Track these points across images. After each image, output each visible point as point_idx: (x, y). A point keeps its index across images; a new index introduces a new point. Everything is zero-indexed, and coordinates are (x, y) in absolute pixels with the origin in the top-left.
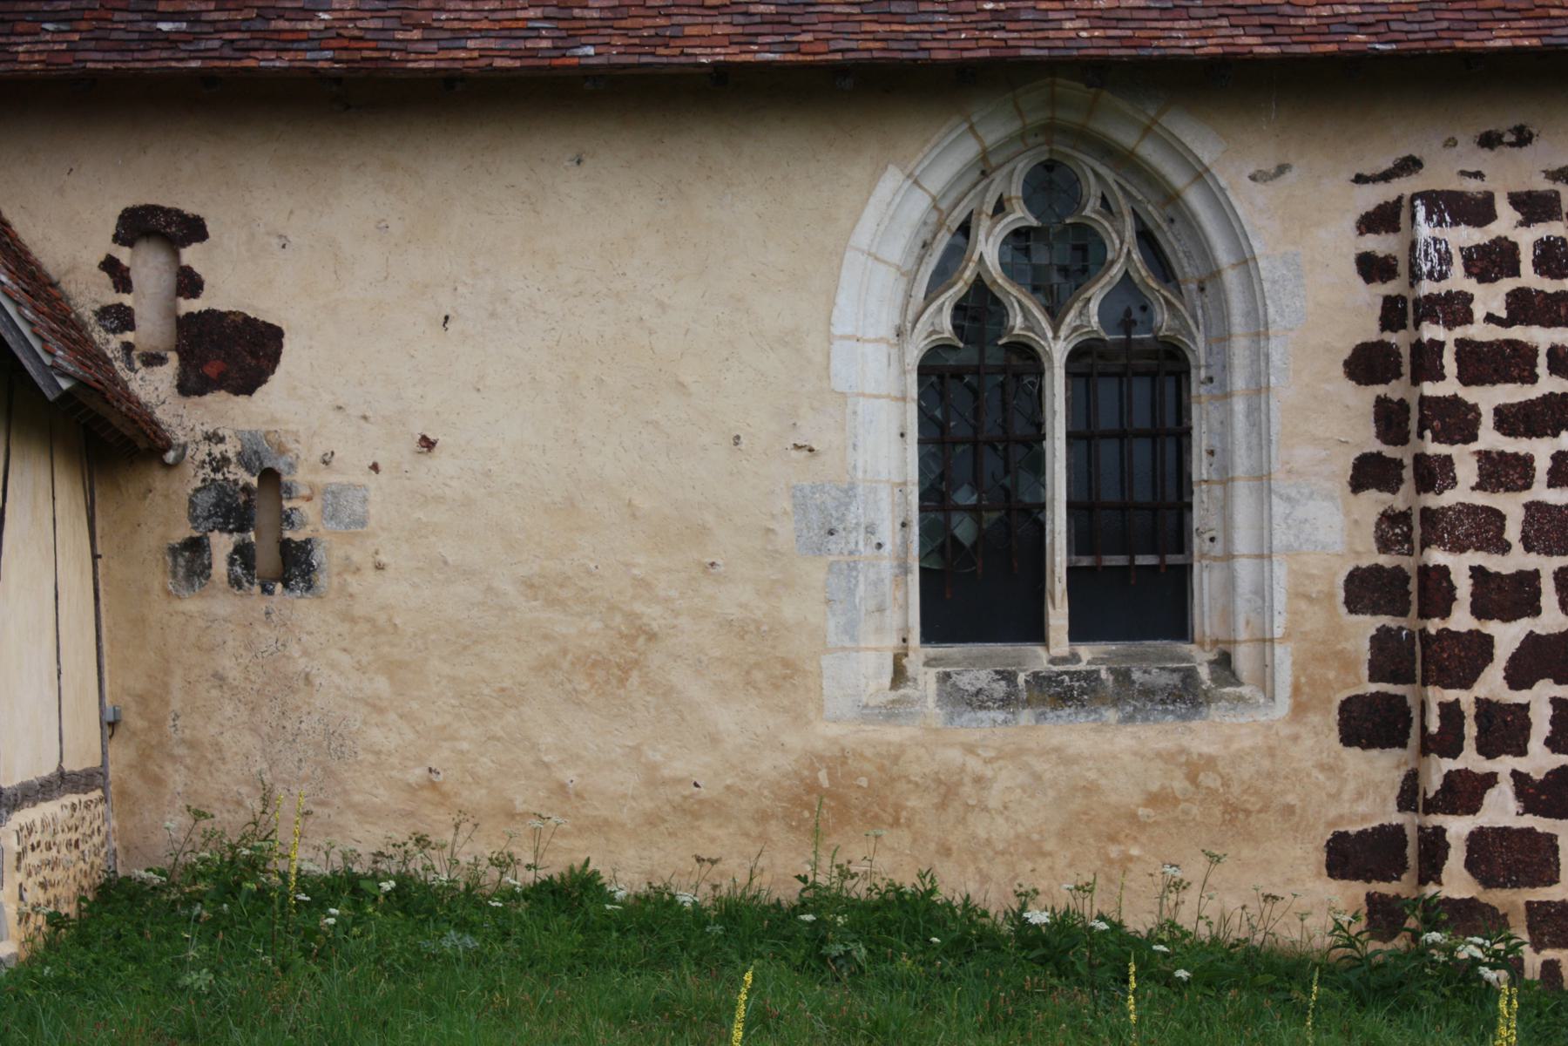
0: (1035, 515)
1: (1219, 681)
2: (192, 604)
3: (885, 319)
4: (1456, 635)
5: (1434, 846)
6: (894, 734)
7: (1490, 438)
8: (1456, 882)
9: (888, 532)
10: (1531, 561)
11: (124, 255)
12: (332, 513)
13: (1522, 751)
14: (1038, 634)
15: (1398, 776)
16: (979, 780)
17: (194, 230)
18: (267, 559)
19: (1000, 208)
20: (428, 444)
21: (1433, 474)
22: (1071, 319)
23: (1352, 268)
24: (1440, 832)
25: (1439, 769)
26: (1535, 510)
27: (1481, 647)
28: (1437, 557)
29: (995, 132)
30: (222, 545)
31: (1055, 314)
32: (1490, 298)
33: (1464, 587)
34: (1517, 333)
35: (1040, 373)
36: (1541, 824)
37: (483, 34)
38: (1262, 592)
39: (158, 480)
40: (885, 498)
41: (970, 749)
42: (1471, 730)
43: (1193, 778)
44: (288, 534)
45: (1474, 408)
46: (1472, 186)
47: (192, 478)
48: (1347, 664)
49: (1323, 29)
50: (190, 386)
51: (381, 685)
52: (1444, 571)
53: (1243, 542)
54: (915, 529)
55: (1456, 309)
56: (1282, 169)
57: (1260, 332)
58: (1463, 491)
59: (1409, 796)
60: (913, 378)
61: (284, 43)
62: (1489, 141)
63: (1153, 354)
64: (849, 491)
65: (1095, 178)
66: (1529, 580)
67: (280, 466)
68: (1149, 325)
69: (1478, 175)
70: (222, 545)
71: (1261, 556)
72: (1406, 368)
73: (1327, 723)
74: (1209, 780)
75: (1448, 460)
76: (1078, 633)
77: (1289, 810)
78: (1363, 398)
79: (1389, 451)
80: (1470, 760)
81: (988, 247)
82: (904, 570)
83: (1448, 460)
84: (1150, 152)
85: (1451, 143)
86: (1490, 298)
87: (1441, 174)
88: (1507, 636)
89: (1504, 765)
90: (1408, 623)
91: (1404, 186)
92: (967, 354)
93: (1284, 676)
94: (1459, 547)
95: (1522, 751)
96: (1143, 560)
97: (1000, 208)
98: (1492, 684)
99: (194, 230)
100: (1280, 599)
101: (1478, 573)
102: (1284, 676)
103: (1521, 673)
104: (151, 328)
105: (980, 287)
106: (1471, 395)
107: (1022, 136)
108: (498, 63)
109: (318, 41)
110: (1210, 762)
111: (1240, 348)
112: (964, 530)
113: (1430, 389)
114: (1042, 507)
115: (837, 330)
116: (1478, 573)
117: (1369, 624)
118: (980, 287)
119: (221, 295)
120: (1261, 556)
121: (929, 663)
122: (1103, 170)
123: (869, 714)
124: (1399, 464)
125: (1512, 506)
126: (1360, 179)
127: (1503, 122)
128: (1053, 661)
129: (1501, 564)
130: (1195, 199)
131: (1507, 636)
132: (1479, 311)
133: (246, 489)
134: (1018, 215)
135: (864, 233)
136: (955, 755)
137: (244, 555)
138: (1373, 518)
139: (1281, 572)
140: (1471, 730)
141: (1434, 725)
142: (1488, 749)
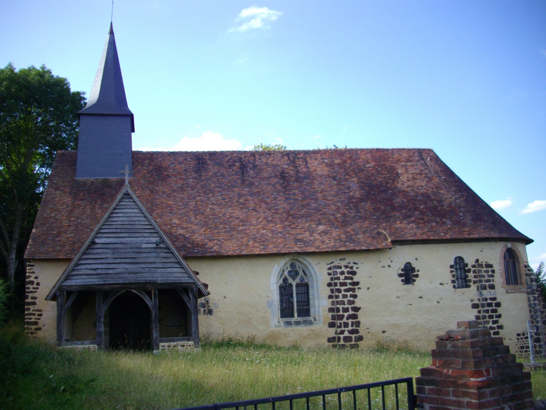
0: (292, 303)
1: (314, 321)
3: (275, 282)
4: (340, 315)
5: (339, 339)
6: (279, 329)
7: (343, 293)
8: (342, 342)
9: (277, 306)
10: (488, 308)
13: (348, 327)
14: (293, 316)
15: (335, 331)
16: (289, 333)
18: (207, 311)
19: (287, 268)
20: (225, 297)
21: (337, 297)
22: (296, 281)
23: (327, 274)
24: (340, 337)
26: (348, 301)
27: (343, 316)
28: (338, 306)
32: (342, 277)
33: (341, 309)
34: (345, 281)
35: (292, 287)
37: (232, 251)
38: (319, 311)
40: (277, 302)
41: (288, 330)
42: (343, 325)
43: (312, 332)
44: (209, 308)
45: (341, 289)
46: (339, 265)
52: (339, 308)
53: (316, 305)
54: (279, 305)
55: (338, 278)
56: (319, 263)
57: (317, 281)
58: (341, 299)
59: (336, 333)
60: (278, 288)
62: (341, 260)
63: (304, 284)
65: (298, 264)
66: (348, 308)
67: (208, 300)
68: (304, 281)
69: (340, 263)
71: (318, 307)
72: (333, 285)
73: (327, 325)
74: (314, 332)
75: (339, 295)
76: (299, 316)
77: (323, 335)
78: (329, 289)
79: (332, 294)
80: (343, 328)
81: (286, 273)
82: (278, 310)
83: (339, 295)
84: (304, 262)
85: (337, 260)
86: (342, 277)
87: (336, 264)
88: (346, 314)
89: (346, 329)
90: (335, 314)
91: (332, 265)
92: (284, 285)
93: (322, 320)
94: (340, 305)
95: (348, 327)
96: (305, 308)
97: (287, 268)
98: (345, 320)
100: (321, 312)
101: (343, 308)
102: (322, 320)
103: (348, 318)
107: (290, 260)
108: (234, 254)
110: (314, 330)
111: (315, 284)
113: (336, 287)
114: (293, 302)
115: (271, 283)
116: (343, 308)
117: (331, 314)
120: (318, 307)
121: (282, 320)
122: (299, 264)
123: (276, 326)
124: (333, 296)
125: (346, 300)
126: (327, 264)
128: (296, 319)
129: (491, 308)
130: (309, 267)
131: (346, 314)
132: (341, 278)
133: (205, 303)
134: (290, 269)
136: (286, 331)
137: (204, 311)
138: (331, 302)
139: (321, 308)
140: (343, 325)
141: (339, 325)
142: (345, 327)
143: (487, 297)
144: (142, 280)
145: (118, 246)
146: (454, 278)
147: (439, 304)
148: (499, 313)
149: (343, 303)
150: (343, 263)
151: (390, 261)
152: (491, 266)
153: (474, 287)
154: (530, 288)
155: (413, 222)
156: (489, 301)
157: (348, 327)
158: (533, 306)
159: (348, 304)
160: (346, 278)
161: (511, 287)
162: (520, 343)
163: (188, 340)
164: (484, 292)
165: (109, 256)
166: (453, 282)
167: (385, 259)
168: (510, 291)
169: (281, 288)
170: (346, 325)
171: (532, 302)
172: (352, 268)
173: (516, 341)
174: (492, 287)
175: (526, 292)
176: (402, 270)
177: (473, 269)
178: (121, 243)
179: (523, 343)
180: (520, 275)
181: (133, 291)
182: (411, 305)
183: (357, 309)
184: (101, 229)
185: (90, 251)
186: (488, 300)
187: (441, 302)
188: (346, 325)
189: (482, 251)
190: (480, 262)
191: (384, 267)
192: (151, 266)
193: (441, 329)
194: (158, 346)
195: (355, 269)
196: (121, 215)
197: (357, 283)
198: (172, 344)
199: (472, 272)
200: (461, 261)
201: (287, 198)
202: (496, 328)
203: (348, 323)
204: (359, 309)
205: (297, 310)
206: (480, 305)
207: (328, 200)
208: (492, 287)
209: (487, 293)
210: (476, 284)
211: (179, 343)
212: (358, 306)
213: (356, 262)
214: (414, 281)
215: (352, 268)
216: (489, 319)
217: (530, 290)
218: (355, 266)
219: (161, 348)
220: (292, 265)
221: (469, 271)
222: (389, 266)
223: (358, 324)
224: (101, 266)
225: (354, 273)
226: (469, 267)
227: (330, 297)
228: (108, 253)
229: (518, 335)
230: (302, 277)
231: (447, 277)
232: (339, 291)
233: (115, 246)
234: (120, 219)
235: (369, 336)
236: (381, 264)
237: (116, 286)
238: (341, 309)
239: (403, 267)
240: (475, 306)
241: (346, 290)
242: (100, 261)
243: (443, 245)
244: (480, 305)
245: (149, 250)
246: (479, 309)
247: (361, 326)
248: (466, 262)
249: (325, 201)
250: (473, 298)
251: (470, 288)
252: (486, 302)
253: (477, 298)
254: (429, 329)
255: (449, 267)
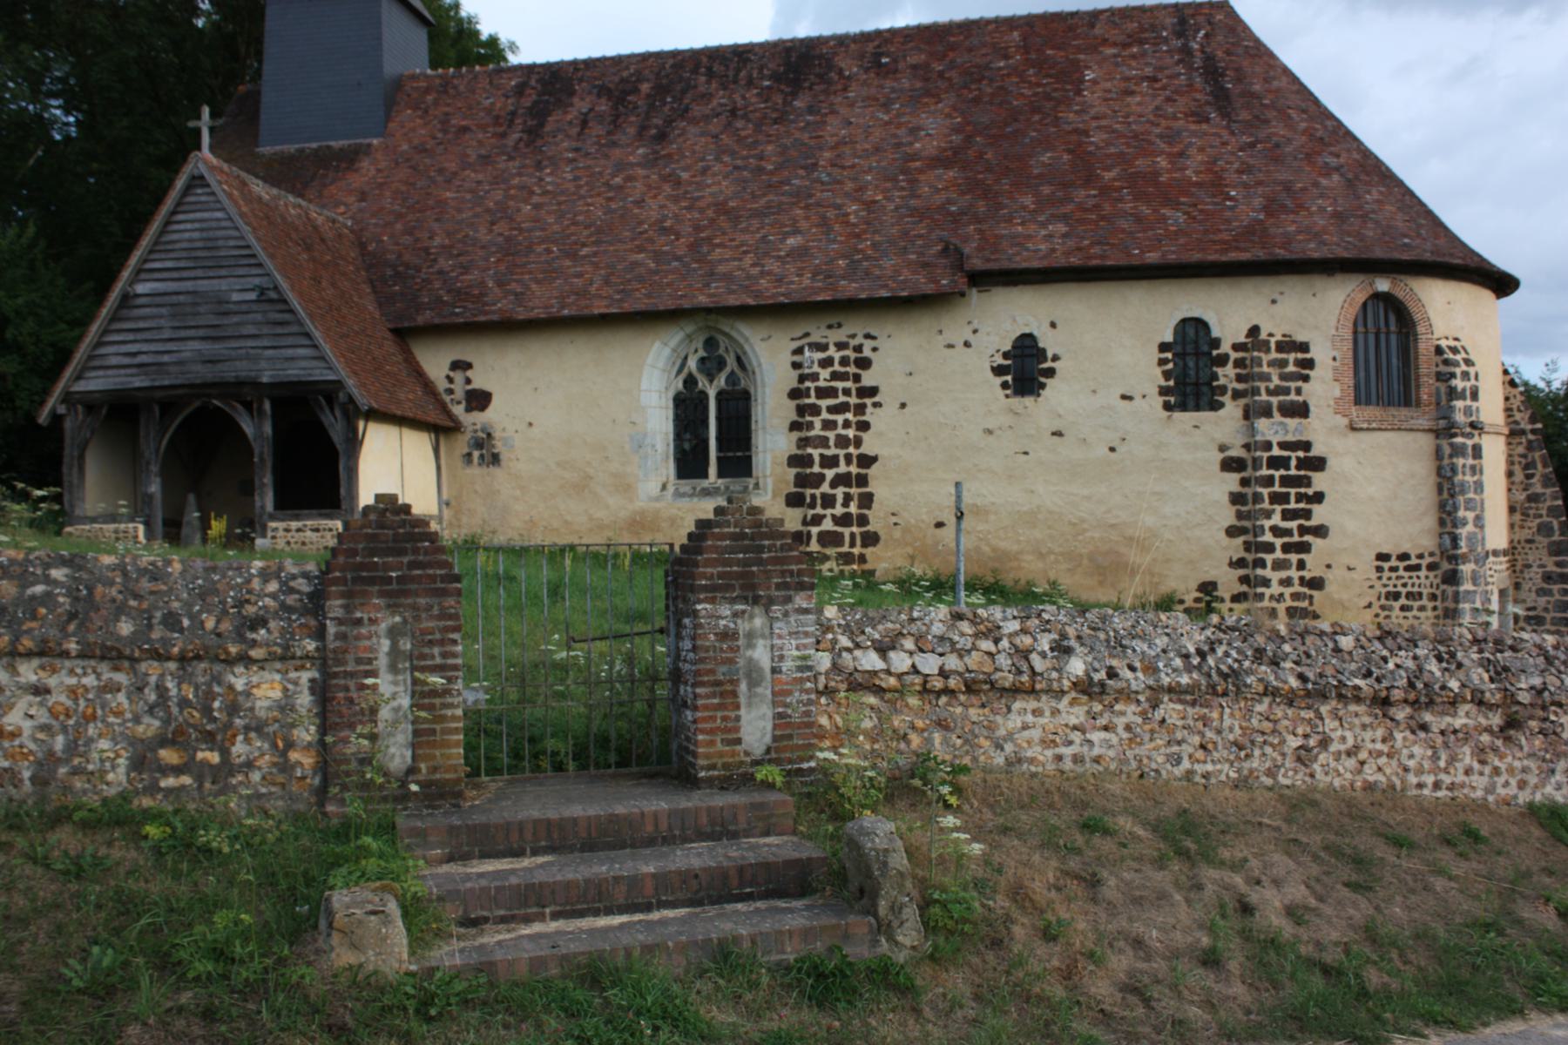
2: (469, 471)
6: (658, 505)
7: (825, 415)
8: (814, 547)
10: (1271, 472)
11: (452, 374)
12: (505, 445)
14: (706, 476)
17: (469, 366)
18: (488, 458)
20: (531, 424)
21: (810, 426)
25: (811, 512)
26: (838, 436)
27: (822, 477)
28: (810, 450)
29: (690, 328)
30: (476, 454)
31: (711, 381)
32: (825, 374)
33: (817, 459)
34: (833, 384)
36: (839, 529)
39: (460, 437)
42: (819, 501)
46: (824, 341)
47: (468, 436)
48: (787, 483)
49: (774, 296)
50: (469, 409)
51: (518, 492)
57: (764, 386)
58: (817, 431)
59: (805, 523)
61: (486, 313)
62: (830, 327)
64: (645, 435)
65: (722, 340)
66: (836, 457)
70: (476, 454)
73: (782, 500)
76: (721, 475)
78: (793, 404)
80: (819, 510)
81: (692, 364)
84: (734, 334)
86: (825, 374)
87: (815, 338)
88: (830, 474)
89: (829, 512)
94: (815, 447)
98: (825, 488)
99: (469, 366)
101: (822, 456)
103: (834, 485)
104: (459, 393)
105: (690, 375)
106: (819, 402)
109: (494, 312)
112: (687, 446)
116: (822, 456)
117: (794, 471)
118: (690, 375)
119: (476, 385)
123: (651, 499)
125: (831, 435)
127: (834, 321)
129: (1282, 472)
131: (830, 474)
134: (702, 353)
135: (649, 361)
136: (674, 511)
137: (482, 456)
140: (819, 501)
142: (824, 506)
143: (1268, 438)
144: (230, 376)
145: (182, 298)
146: (1167, 379)
147: (1112, 455)
148: (1318, 489)
149: (824, 442)
150: (839, 335)
151: (969, 330)
152: (1304, 347)
153: (1232, 409)
154: (1444, 418)
155: (1065, 218)
156: (1276, 452)
157: (833, 507)
158: (1449, 474)
159: (836, 446)
160: (835, 376)
161: (1372, 412)
162: (1384, 581)
163: (330, 517)
164: (1262, 424)
165: (162, 322)
166: (1163, 391)
167: (954, 326)
168: (1365, 426)
169: (679, 401)
170: (829, 501)
171: (1446, 462)
172: (858, 349)
173: (1374, 575)
174: (1301, 410)
175: (1430, 430)
176: (1006, 355)
177: (1234, 355)
178: (188, 293)
179: (1399, 582)
180: (1418, 377)
181: (215, 402)
182: (1026, 453)
183: (867, 461)
184: (146, 261)
185: (124, 312)
186: (1275, 447)
187: (1121, 449)
188: (829, 501)
189: (1274, 302)
190: (1263, 336)
191: (950, 346)
192: (250, 343)
193: (1112, 526)
194: (264, 528)
195: (867, 352)
196: (189, 226)
197: (873, 391)
198: (294, 525)
199: (1230, 364)
200: (1202, 334)
201: (736, 168)
202: (1295, 532)
203: (834, 496)
204: (874, 459)
205: (719, 459)
206: (1249, 463)
207: (843, 168)
208: (1301, 410)
209: (1272, 429)
210: (1243, 401)
211: (309, 523)
212: (871, 453)
213: (873, 333)
214: (1043, 386)
215: (858, 349)
216: (1271, 503)
217: (1442, 423)
218: (868, 344)
219: (270, 534)
220: (710, 344)
221: (1222, 360)
222: (967, 344)
223: (867, 500)
224: (145, 347)
225: (864, 363)
226: (1225, 348)
227: (795, 426)
228: (161, 317)
229: (1383, 557)
230: (732, 373)
231: (1149, 375)
232: (815, 410)
233: (174, 299)
234: (187, 235)
235: (897, 534)
236: (941, 340)
237: (180, 392)
238: (817, 459)
239: (1007, 347)
240: (1230, 465)
241: (833, 410)
242: (139, 336)
243: (1145, 284)
244: (1249, 463)
245: (244, 307)
246: (1244, 474)
247: (874, 505)
248: (1215, 333)
249: (836, 171)
250: (1226, 440)
251: (1221, 412)
252: (1266, 455)
253: (1241, 440)
254: (1074, 525)
255: (1156, 349)
